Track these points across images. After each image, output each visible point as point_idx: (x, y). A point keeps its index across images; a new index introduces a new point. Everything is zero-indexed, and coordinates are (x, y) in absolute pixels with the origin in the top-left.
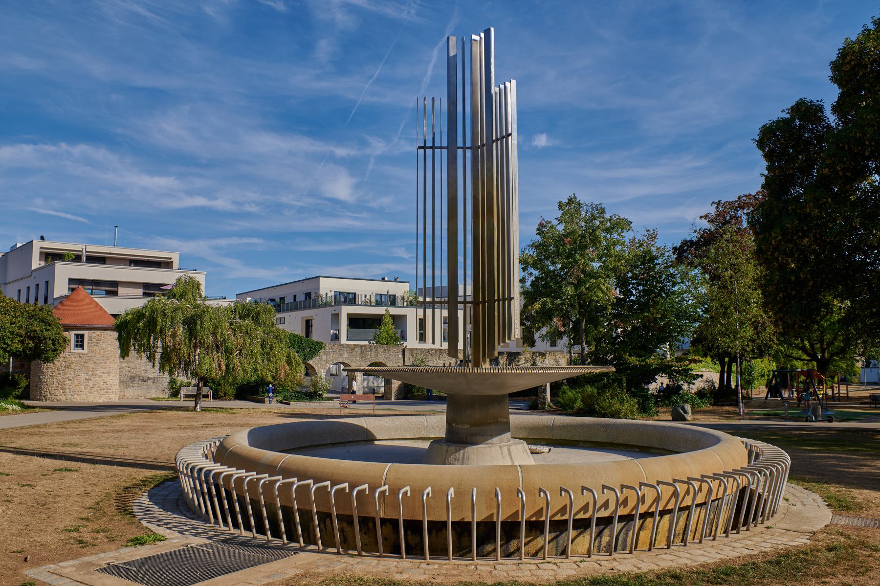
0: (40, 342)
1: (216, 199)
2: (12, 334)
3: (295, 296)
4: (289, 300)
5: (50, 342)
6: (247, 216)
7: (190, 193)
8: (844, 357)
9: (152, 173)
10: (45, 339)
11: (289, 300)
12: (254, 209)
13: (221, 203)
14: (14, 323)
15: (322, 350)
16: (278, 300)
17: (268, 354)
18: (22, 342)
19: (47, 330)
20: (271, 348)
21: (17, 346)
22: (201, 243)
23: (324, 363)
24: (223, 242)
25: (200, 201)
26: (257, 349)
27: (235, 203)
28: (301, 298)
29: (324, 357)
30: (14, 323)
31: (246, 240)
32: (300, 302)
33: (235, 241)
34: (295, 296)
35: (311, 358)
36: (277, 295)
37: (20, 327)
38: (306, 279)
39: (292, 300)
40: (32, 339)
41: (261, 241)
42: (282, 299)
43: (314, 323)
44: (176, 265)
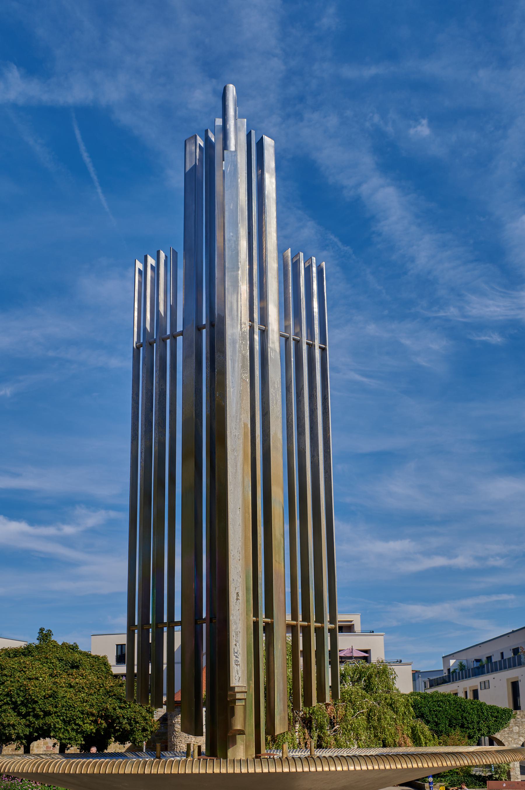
0: (114, 721)
1: (456, 556)
2: (82, 713)
3: (502, 654)
4: (496, 658)
5: (126, 721)
6: (493, 570)
7: (428, 554)
8: (304, 728)
9: (386, 539)
10: (118, 718)
11: (496, 658)
12: (499, 563)
13: (461, 561)
14: (87, 701)
15: (512, 720)
16: (484, 660)
17: (375, 728)
18: (95, 722)
19: (120, 708)
20: (379, 720)
21: (89, 728)
22: (447, 605)
23: (516, 736)
24: (469, 602)
25: (440, 561)
26: (362, 721)
27: (477, 558)
28: (509, 654)
29: (516, 729)
30: (87, 701)
31: (494, 598)
32: (509, 659)
33: (483, 600)
34: (502, 654)
35: (498, 730)
36: (482, 654)
37: (92, 706)
38: (513, 632)
39: (499, 658)
40: (106, 718)
41: (512, 597)
42: (489, 658)
43: (521, 685)
44: (358, 628)
